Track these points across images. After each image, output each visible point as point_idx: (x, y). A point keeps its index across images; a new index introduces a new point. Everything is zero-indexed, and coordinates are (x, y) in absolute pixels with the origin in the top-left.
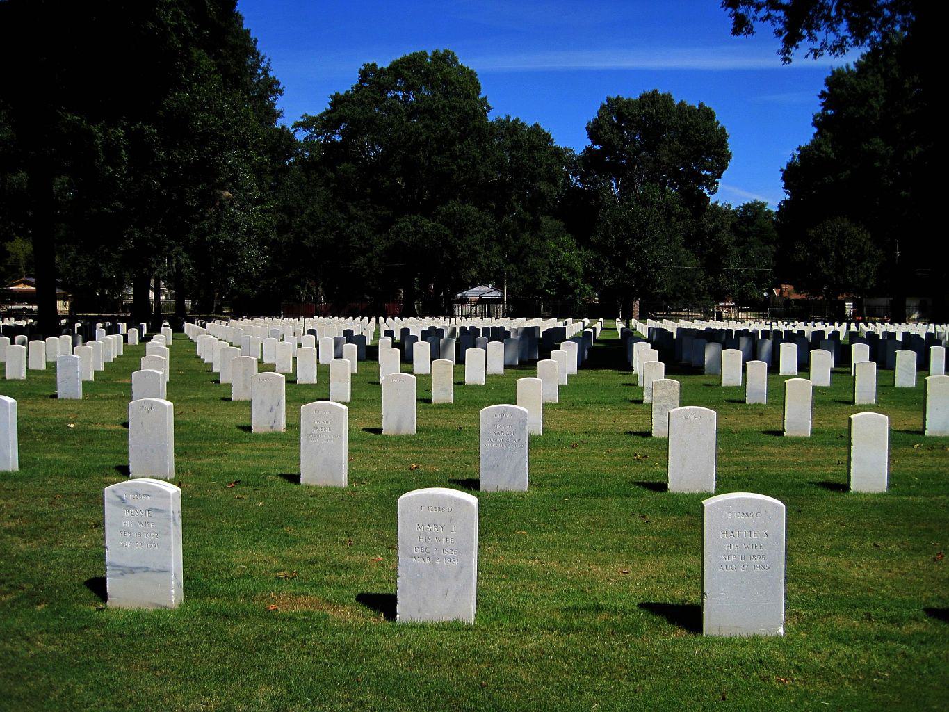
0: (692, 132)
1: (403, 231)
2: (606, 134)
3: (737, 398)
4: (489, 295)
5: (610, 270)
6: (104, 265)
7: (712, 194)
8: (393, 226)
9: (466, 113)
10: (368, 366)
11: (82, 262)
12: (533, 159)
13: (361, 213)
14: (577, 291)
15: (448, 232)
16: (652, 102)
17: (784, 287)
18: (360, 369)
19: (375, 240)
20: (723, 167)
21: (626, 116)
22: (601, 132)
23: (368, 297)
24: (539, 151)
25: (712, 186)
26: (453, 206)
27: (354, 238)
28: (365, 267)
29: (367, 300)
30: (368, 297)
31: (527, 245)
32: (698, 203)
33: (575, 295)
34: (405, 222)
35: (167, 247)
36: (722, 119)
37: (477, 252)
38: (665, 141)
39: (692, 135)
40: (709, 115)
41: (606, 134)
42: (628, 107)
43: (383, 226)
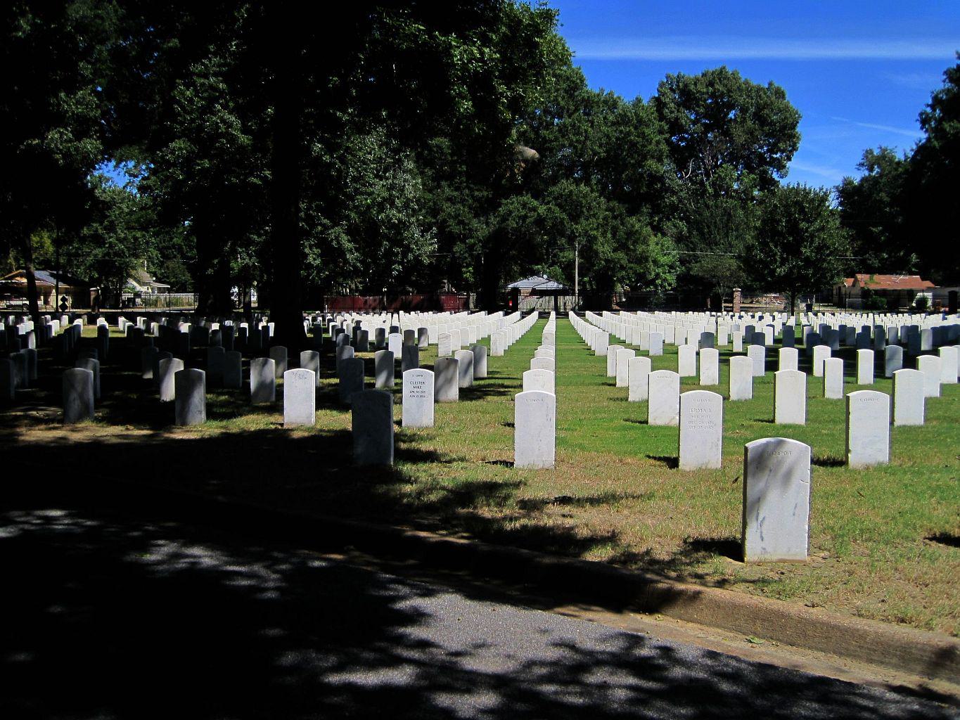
0: (766, 111)
1: (513, 215)
2: (672, 112)
3: (611, 382)
4: (543, 287)
5: (781, 257)
6: (244, 249)
7: (782, 177)
8: (500, 209)
9: (574, 82)
10: (770, 374)
11: (86, 252)
12: (643, 135)
13: (456, 194)
14: (659, 282)
15: (564, 216)
16: (720, 80)
17: (859, 276)
18: (948, 386)
19: (475, 223)
20: (794, 148)
21: (694, 94)
22: (667, 111)
23: (411, 290)
24: (648, 126)
25: (780, 166)
26: (565, 186)
27: (451, 222)
28: (467, 255)
29: (410, 292)
30: (411, 290)
31: (637, 231)
32: (767, 183)
33: (656, 286)
34: (513, 204)
35: (320, 228)
36: (792, 101)
37: (595, 238)
38: (733, 123)
39: (767, 115)
40: (780, 94)
41: (672, 112)
42: (695, 84)
43: (484, 208)
